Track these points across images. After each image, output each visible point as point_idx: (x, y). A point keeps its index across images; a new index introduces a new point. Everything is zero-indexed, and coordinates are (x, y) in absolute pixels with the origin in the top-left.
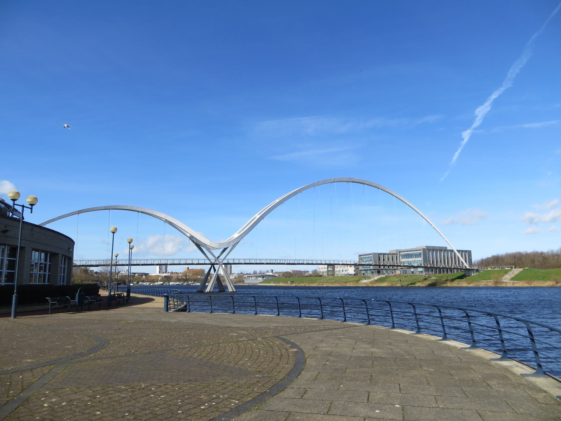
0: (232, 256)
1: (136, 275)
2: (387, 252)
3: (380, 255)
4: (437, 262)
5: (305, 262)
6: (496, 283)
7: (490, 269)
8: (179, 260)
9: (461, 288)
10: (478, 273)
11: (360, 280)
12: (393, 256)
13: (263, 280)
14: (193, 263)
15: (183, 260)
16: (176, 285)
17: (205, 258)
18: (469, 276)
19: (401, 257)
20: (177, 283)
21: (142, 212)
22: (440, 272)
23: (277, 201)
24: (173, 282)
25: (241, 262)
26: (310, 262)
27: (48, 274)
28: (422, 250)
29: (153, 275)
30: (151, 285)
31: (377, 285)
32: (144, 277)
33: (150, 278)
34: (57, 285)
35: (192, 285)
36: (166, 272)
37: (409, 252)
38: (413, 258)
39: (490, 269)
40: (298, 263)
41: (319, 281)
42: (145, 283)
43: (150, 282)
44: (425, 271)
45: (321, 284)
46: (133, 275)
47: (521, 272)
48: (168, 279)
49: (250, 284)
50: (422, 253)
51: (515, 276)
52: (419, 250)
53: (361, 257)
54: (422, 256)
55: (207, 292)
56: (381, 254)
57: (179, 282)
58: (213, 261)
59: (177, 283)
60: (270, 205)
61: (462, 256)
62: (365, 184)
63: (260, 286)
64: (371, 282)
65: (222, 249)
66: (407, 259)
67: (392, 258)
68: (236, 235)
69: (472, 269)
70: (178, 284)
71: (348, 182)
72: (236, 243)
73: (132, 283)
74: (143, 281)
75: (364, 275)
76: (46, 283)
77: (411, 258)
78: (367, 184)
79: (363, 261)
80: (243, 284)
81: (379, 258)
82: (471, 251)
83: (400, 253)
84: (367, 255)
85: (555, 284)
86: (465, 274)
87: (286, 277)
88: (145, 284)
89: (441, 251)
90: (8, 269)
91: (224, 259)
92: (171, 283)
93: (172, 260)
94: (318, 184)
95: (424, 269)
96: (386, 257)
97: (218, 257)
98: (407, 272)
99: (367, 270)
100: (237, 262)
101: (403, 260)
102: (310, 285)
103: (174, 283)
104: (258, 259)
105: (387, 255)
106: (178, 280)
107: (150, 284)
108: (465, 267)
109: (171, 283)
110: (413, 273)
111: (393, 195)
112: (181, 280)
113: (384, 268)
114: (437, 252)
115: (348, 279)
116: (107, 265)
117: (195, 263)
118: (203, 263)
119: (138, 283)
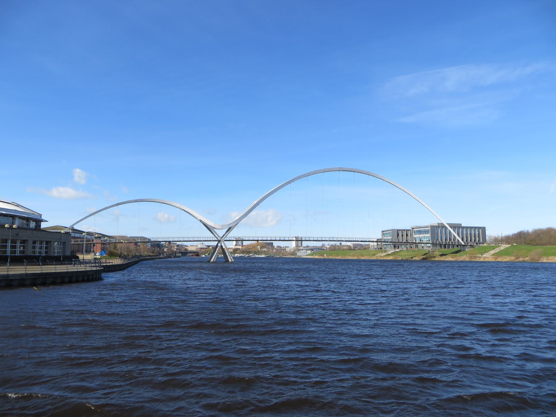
1: (211, 247)
3: (399, 232)
4: (446, 240)
5: (312, 239)
8: (248, 237)
14: (276, 239)
16: (240, 256)
17: (213, 236)
19: (414, 233)
21: (162, 203)
22: (445, 248)
25: (310, 239)
27: (45, 246)
28: (430, 227)
31: (385, 258)
34: (66, 255)
35: (252, 256)
38: (424, 234)
44: (433, 246)
47: (507, 248)
51: (499, 251)
53: (383, 233)
55: (211, 262)
56: (400, 230)
58: (219, 239)
62: (355, 172)
63: (305, 258)
70: (241, 256)
71: (339, 171)
72: (237, 223)
73: (204, 255)
79: (385, 237)
81: (398, 234)
82: (485, 227)
83: (414, 230)
85: (515, 259)
89: (459, 228)
90: (46, 245)
93: (248, 237)
95: (431, 245)
99: (388, 245)
102: (336, 258)
103: (238, 255)
104: (308, 237)
105: (405, 231)
110: (423, 247)
111: (384, 180)
113: (341, 242)
114: (463, 229)
117: (278, 240)
118: (308, 239)
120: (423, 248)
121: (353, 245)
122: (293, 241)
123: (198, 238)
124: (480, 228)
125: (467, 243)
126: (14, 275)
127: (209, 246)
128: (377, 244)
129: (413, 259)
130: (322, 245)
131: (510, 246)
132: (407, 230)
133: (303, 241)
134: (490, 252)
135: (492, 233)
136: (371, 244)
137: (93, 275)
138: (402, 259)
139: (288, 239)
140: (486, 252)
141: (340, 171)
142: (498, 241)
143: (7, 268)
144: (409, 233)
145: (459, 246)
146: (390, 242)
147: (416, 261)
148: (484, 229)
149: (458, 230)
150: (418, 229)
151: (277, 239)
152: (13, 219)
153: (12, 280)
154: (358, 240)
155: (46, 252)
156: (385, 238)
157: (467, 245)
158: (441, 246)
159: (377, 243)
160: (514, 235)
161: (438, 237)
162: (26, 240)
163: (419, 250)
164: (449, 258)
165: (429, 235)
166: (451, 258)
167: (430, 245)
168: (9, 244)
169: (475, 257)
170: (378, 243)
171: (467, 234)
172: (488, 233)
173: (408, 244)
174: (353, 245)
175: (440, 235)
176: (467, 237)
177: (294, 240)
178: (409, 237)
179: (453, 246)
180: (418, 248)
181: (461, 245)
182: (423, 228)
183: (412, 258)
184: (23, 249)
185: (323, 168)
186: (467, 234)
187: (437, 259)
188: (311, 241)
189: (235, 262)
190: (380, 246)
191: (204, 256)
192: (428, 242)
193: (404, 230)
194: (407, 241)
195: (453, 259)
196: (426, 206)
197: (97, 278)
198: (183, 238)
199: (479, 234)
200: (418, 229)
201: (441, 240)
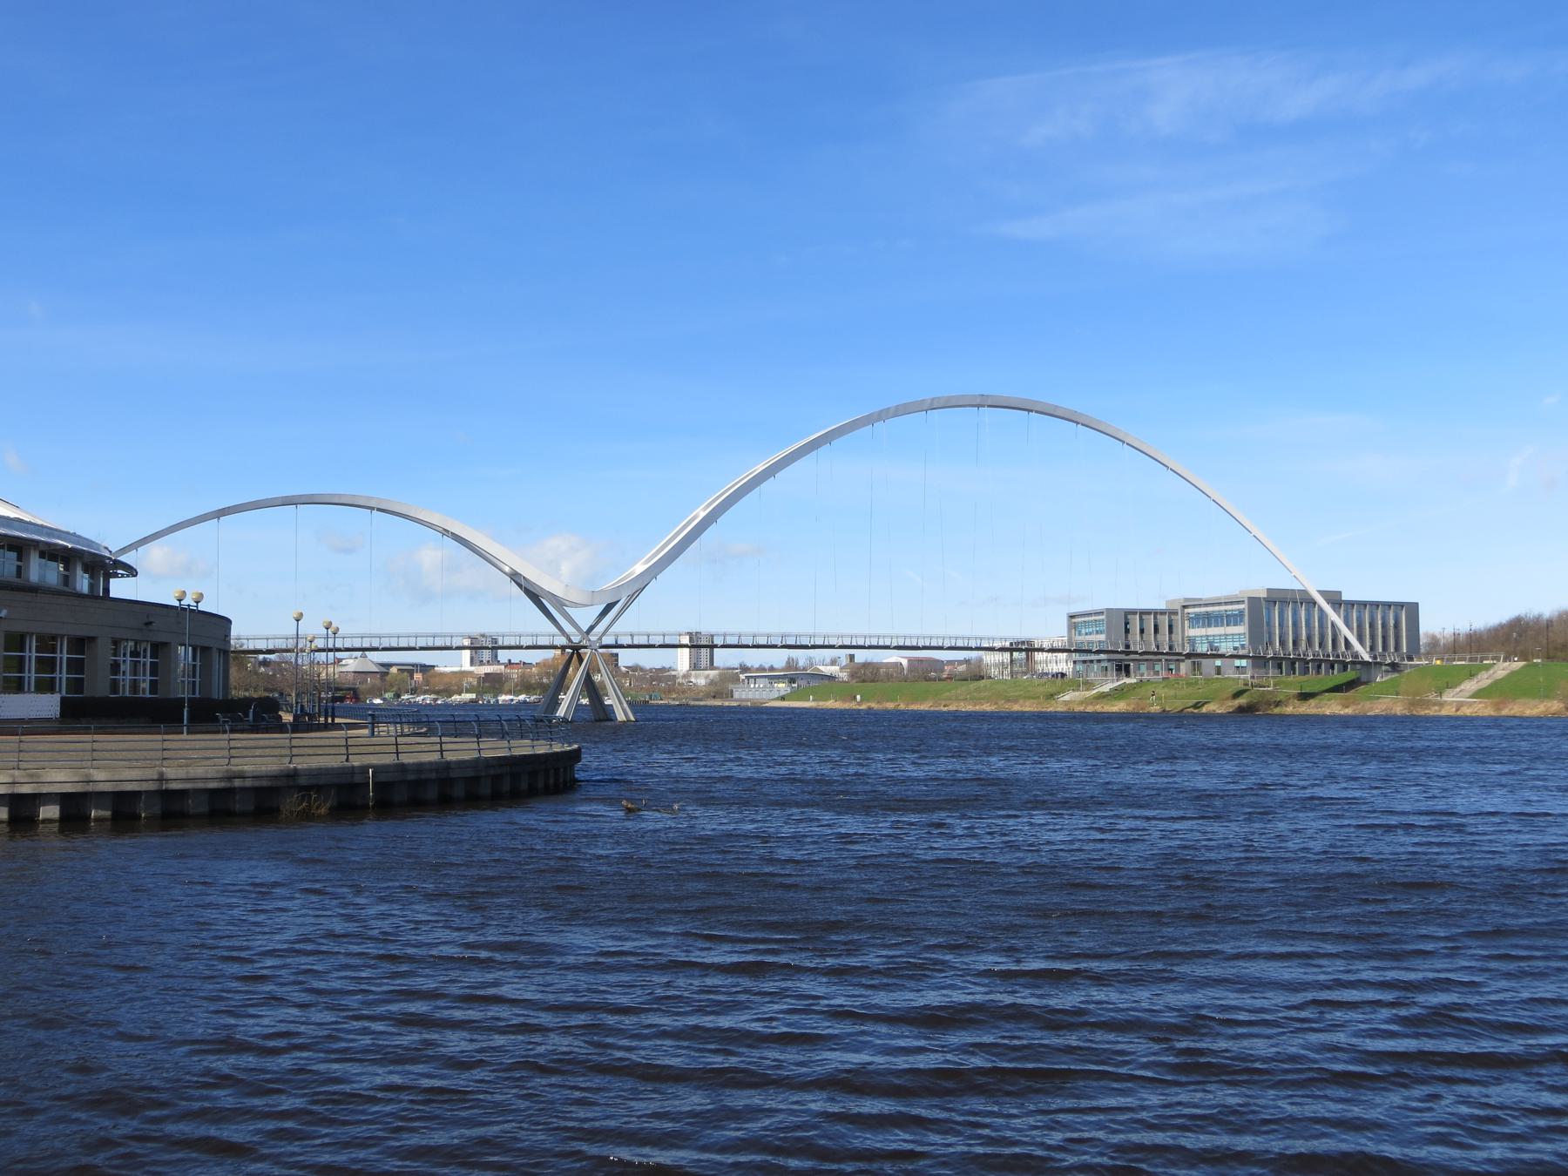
0: (628, 625)
1: (394, 670)
2: (1161, 605)
3: (1129, 617)
4: (1295, 643)
5: (658, 640)
6: (1413, 704)
7: (1438, 662)
9: (1321, 720)
10: (1396, 675)
11: (1059, 693)
12: (1173, 617)
13: (789, 689)
15: (762, 635)
17: (554, 630)
18: (1365, 683)
20: (522, 697)
23: (760, 468)
24: (511, 694)
25: (745, 643)
26: (763, 641)
29: (448, 669)
30: (439, 702)
31: (1098, 708)
32: (418, 676)
33: (437, 679)
36: (712, 666)
37: (1210, 609)
38: (1222, 626)
39: (1438, 662)
40: (928, 644)
41: (948, 694)
42: (422, 697)
43: (437, 693)
44: (1254, 666)
45: (944, 703)
46: (384, 670)
47: (1513, 674)
48: (494, 683)
49: (744, 704)
50: (1246, 611)
52: (1238, 602)
53: (1074, 620)
54: (1246, 619)
56: (1133, 612)
57: (527, 693)
58: (576, 639)
59: (522, 697)
60: (736, 484)
61: (1347, 623)
62: (1032, 411)
64: (1085, 701)
65: (603, 606)
66: (1204, 630)
67: (1170, 627)
68: (639, 568)
69: (1376, 663)
71: (979, 406)
72: (638, 587)
73: (380, 696)
74: (414, 691)
75: (1219, 673)
76: (197, 695)
77: (1216, 626)
78: (1037, 412)
79: (1080, 634)
80: (727, 704)
82: (1417, 604)
83: (1186, 610)
84: (1089, 614)
86: (1358, 679)
87: (864, 681)
88: (419, 699)
91: (604, 634)
92: (503, 698)
94: (882, 416)
95: (1250, 661)
96: (1164, 621)
97: (592, 628)
98: (1204, 669)
99: (1092, 661)
100: (730, 641)
101: (1192, 632)
103: (511, 697)
106: (526, 687)
107: (435, 700)
108: (1356, 655)
109: (503, 698)
110: (1218, 670)
112: (534, 689)
114: (1271, 608)
115: (1030, 689)
116: (287, 651)
117: (658, 644)
119: (398, 696)
120: (1219, 673)
121: (910, 660)
122: (679, 649)
123: (664, 636)
124: (1402, 607)
125: (1375, 658)
126: (311, 773)
127: (390, 665)
128: (1012, 661)
129: (1204, 710)
130: (788, 662)
131: (1523, 667)
132: (1156, 613)
133: (716, 646)
134: (1462, 687)
135: (1436, 623)
136: (990, 658)
137: (497, 778)
138: (1164, 711)
139: (630, 643)
140: (1449, 686)
141: (983, 406)
142: (1478, 646)
143: (160, 747)
144: (1164, 621)
145: (1336, 666)
146: (1098, 652)
147: (1210, 717)
148: (1412, 609)
149: (1346, 611)
150: (1203, 609)
151: (745, 641)
152: (19, 558)
153: (183, 793)
154: (888, 643)
155: (154, 686)
156: (1079, 638)
157: (1380, 664)
158: (1280, 666)
159: (1012, 655)
160: (1489, 630)
161: (1271, 635)
162: (89, 638)
163: (1208, 681)
164: (1333, 707)
165: (1242, 629)
166: (1339, 708)
167: (1244, 663)
168: (32, 654)
169: (1427, 704)
170: (1016, 654)
171: (1296, 624)
172: (234, 632)
173: (1160, 660)
174: (910, 660)
175: (1382, 632)
176: (1373, 637)
177: (487, 648)
178: (1177, 637)
179: (1345, 666)
180: (1201, 674)
181: (1358, 662)
182: (1219, 604)
183: (1196, 706)
184: (599, 671)
185: (928, 396)
186: (1296, 624)
187: (1289, 710)
188: (653, 646)
189: (637, 721)
190: (1021, 666)
191: (378, 701)
192: (1241, 652)
193: (1148, 612)
194: (1128, 646)
195: (1349, 711)
196: (1256, 531)
197: (561, 786)
198: (267, 639)
199: (1397, 626)
200: (1203, 609)
201: (1283, 643)
